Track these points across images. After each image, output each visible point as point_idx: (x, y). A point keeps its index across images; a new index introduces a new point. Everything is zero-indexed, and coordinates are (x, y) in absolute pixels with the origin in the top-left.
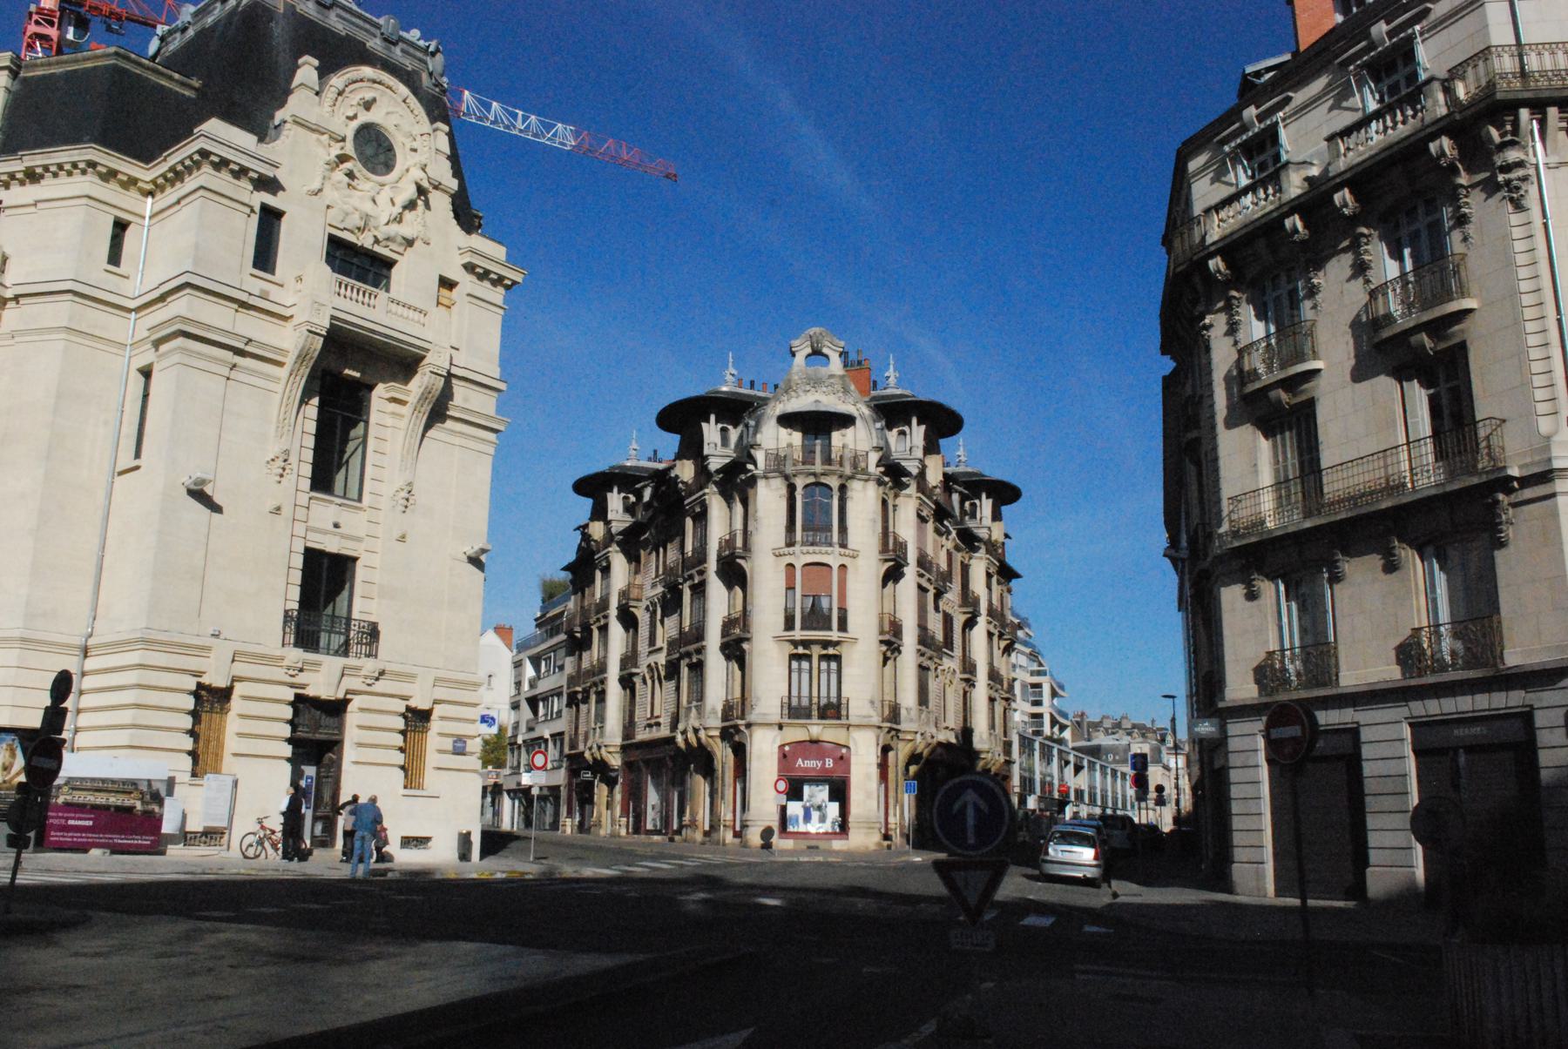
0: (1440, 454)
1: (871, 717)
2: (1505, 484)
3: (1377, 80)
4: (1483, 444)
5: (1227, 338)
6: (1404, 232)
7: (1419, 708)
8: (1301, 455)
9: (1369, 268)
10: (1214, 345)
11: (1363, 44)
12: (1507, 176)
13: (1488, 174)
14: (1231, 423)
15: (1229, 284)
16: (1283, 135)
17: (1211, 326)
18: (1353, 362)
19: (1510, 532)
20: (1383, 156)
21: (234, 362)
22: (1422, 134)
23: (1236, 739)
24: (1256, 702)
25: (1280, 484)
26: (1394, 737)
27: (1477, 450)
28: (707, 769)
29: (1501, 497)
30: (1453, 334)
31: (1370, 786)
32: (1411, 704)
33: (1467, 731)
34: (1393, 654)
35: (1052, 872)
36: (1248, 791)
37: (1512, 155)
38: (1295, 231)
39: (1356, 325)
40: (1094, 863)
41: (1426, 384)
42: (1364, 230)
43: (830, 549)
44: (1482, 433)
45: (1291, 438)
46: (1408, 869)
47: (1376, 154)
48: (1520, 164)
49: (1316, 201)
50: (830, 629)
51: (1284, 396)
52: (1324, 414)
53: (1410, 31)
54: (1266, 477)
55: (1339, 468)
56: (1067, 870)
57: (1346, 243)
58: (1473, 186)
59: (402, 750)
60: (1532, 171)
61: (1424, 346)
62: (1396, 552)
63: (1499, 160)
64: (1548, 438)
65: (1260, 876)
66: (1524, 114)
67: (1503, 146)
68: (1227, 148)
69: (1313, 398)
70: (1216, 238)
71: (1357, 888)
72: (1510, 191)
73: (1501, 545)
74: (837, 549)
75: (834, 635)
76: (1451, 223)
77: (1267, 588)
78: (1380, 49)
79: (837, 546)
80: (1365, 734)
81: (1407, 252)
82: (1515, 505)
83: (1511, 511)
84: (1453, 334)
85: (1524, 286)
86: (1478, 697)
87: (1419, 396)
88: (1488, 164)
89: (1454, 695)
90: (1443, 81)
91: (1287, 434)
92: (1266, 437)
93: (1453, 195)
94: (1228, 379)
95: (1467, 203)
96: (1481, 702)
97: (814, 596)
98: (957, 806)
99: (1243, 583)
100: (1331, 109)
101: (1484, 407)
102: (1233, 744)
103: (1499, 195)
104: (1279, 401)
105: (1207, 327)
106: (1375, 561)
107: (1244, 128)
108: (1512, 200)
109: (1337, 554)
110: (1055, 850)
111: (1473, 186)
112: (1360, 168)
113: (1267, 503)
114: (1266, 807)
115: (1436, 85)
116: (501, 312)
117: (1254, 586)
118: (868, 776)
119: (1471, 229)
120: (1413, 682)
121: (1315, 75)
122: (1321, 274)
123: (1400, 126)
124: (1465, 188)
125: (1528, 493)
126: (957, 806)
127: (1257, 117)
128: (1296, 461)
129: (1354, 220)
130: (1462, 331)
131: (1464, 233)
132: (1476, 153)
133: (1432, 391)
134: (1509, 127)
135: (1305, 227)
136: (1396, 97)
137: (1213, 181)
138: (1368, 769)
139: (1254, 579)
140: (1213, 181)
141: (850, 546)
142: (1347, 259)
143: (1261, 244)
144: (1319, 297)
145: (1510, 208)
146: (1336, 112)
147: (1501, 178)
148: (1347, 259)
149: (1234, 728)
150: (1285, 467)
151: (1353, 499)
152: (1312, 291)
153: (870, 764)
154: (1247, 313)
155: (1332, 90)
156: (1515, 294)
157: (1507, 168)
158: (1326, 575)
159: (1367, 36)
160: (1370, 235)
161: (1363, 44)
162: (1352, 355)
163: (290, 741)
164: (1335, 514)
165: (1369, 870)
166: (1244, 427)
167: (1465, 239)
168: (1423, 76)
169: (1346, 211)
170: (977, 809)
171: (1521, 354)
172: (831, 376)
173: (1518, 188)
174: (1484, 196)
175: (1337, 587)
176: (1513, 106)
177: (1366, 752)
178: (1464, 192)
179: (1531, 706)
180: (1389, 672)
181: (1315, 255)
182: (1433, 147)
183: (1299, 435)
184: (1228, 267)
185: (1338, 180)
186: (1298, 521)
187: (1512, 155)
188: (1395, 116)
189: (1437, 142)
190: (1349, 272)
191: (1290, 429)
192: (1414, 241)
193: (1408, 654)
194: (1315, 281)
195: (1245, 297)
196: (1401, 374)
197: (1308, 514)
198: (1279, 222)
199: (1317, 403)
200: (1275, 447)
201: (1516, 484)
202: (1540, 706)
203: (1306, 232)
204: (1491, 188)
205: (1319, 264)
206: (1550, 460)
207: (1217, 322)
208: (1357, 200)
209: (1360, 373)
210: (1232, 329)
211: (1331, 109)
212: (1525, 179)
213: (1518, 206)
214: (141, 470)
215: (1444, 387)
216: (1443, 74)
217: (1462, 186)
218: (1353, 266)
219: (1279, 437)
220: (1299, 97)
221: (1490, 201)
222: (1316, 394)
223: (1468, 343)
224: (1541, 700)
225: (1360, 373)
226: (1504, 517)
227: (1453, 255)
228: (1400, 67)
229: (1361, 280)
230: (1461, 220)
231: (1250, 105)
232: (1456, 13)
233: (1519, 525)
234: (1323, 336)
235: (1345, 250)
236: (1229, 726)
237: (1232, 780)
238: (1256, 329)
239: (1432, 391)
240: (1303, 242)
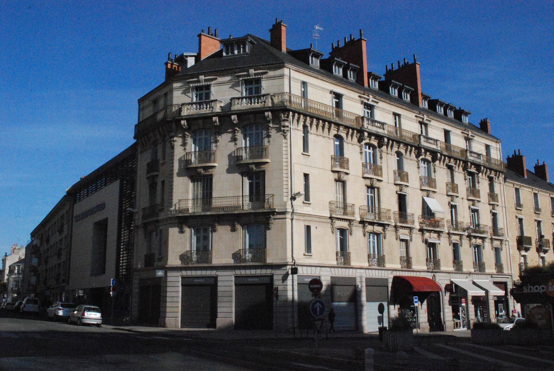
0: (251, 200)
2: (273, 213)
3: (246, 85)
4: (266, 201)
5: (181, 147)
6: (248, 132)
7: (238, 272)
8: (203, 190)
9: (237, 140)
10: (176, 147)
11: (245, 73)
12: (284, 129)
13: (278, 126)
14: (179, 175)
15: (185, 130)
16: (213, 89)
17: (176, 141)
18: (227, 167)
19: (272, 226)
20: (250, 110)
21: (163, 93)
22: (264, 109)
23: (170, 277)
24: (180, 266)
25: (195, 199)
26: (230, 280)
27: (264, 202)
28: (345, 264)
29: (272, 216)
30: (261, 168)
31: (219, 294)
32: (182, 271)
33: (198, 280)
34: (231, 256)
35: (86, 322)
36: (174, 294)
37: (287, 124)
38: (216, 122)
39: (230, 156)
40: (101, 318)
41: (249, 179)
42: (237, 129)
44: (266, 198)
45: (201, 184)
46: (231, 319)
47: (248, 109)
48: (288, 127)
49: (225, 115)
51: (202, 172)
52: (215, 181)
53: (262, 76)
54: (190, 196)
55: (225, 198)
56: (91, 321)
57: (230, 130)
58: (274, 128)
60: (289, 129)
61: (253, 169)
62: (236, 226)
63: (283, 124)
64: (286, 203)
65: (176, 321)
66: (291, 113)
67: (284, 120)
68: (191, 85)
69: (212, 174)
70: (185, 114)
71: (213, 324)
72: (284, 133)
73: (269, 229)
76: (265, 136)
77: (187, 230)
78: (251, 77)
80: (219, 279)
81: (248, 139)
82: (274, 219)
83: (273, 220)
84: (261, 168)
85: (284, 160)
86: (268, 270)
87: (247, 182)
88: (279, 123)
89: (196, 270)
90: (272, 96)
91: (199, 183)
92: (192, 183)
93: (268, 128)
94: (180, 160)
95: (271, 132)
96: (258, 272)
99: (178, 227)
100: (230, 88)
101: (268, 191)
102: (169, 279)
103: (281, 133)
104: (201, 173)
105: (174, 141)
106: (228, 228)
107: (199, 81)
108: (284, 135)
109: (216, 224)
110: (87, 314)
111: (274, 128)
112: (242, 111)
113: (190, 204)
114: (180, 300)
115: (269, 96)
117: (183, 229)
119: (271, 139)
120: (238, 265)
122: (220, 137)
123: (256, 103)
124: (271, 128)
125: (278, 216)
126: (315, 306)
127: (204, 80)
128: (201, 192)
130: (265, 167)
131: (269, 140)
132: (277, 119)
133: (250, 181)
134: (286, 115)
135: (219, 122)
136: (257, 95)
137: (182, 93)
138: (219, 289)
139: (183, 227)
140: (182, 93)
142: (229, 136)
143: (200, 122)
144: (218, 144)
145: (283, 138)
146: (231, 89)
147: (282, 129)
148: (229, 136)
149: (169, 274)
150: (197, 193)
151: (223, 208)
152: (216, 141)
154: (190, 141)
155: (231, 82)
156: (281, 162)
157: (284, 127)
158: (210, 230)
159: (248, 71)
160: (239, 131)
161: (245, 73)
162: (228, 164)
164: (219, 212)
165: (218, 319)
166: (186, 177)
167: (269, 142)
168: (263, 92)
169: (235, 122)
171: (281, 179)
173: (286, 133)
174: (276, 132)
175: (214, 234)
176: (289, 110)
177: (219, 284)
178: (271, 128)
179: (273, 274)
180: (230, 261)
181: (219, 131)
182: (266, 114)
183: (204, 183)
184: (187, 125)
185: (234, 112)
186: (199, 211)
187: (287, 124)
188: (255, 100)
189: (268, 113)
190: (230, 140)
191: (201, 181)
192: (251, 136)
193: (236, 256)
194: (218, 138)
195: (190, 135)
196: (243, 174)
197: (203, 210)
198: (211, 117)
199: (213, 176)
200: (194, 186)
201: (276, 213)
202: (276, 274)
203: (219, 123)
204: (279, 130)
205: (220, 134)
206: (286, 209)
207: (178, 141)
208: (238, 120)
209: (229, 171)
210: (184, 144)
211: (230, 88)
212: (288, 131)
213: (285, 137)
215: (254, 181)
216: (272, 94)
217: (270, 127)
218: (231, 138)
219: (196, 183)
220: (220, 79)
221: (277, 134)
222: (214, 173)
223: (266, 171)
224: (276, 272)
225: (229, 171)
226: (271, 222)
227: (264, 146)
228: (254, 84)
229: (233, 143)
230: (269, 136)
231: (203, 75)
232: (275, 77)
233: (275, 224)
234: (218, 155)
235: (229, 132)
236: (168, 273)
237: (167, 291)
238: (191, 147)
239: (250, 181)
240: (217, 126)
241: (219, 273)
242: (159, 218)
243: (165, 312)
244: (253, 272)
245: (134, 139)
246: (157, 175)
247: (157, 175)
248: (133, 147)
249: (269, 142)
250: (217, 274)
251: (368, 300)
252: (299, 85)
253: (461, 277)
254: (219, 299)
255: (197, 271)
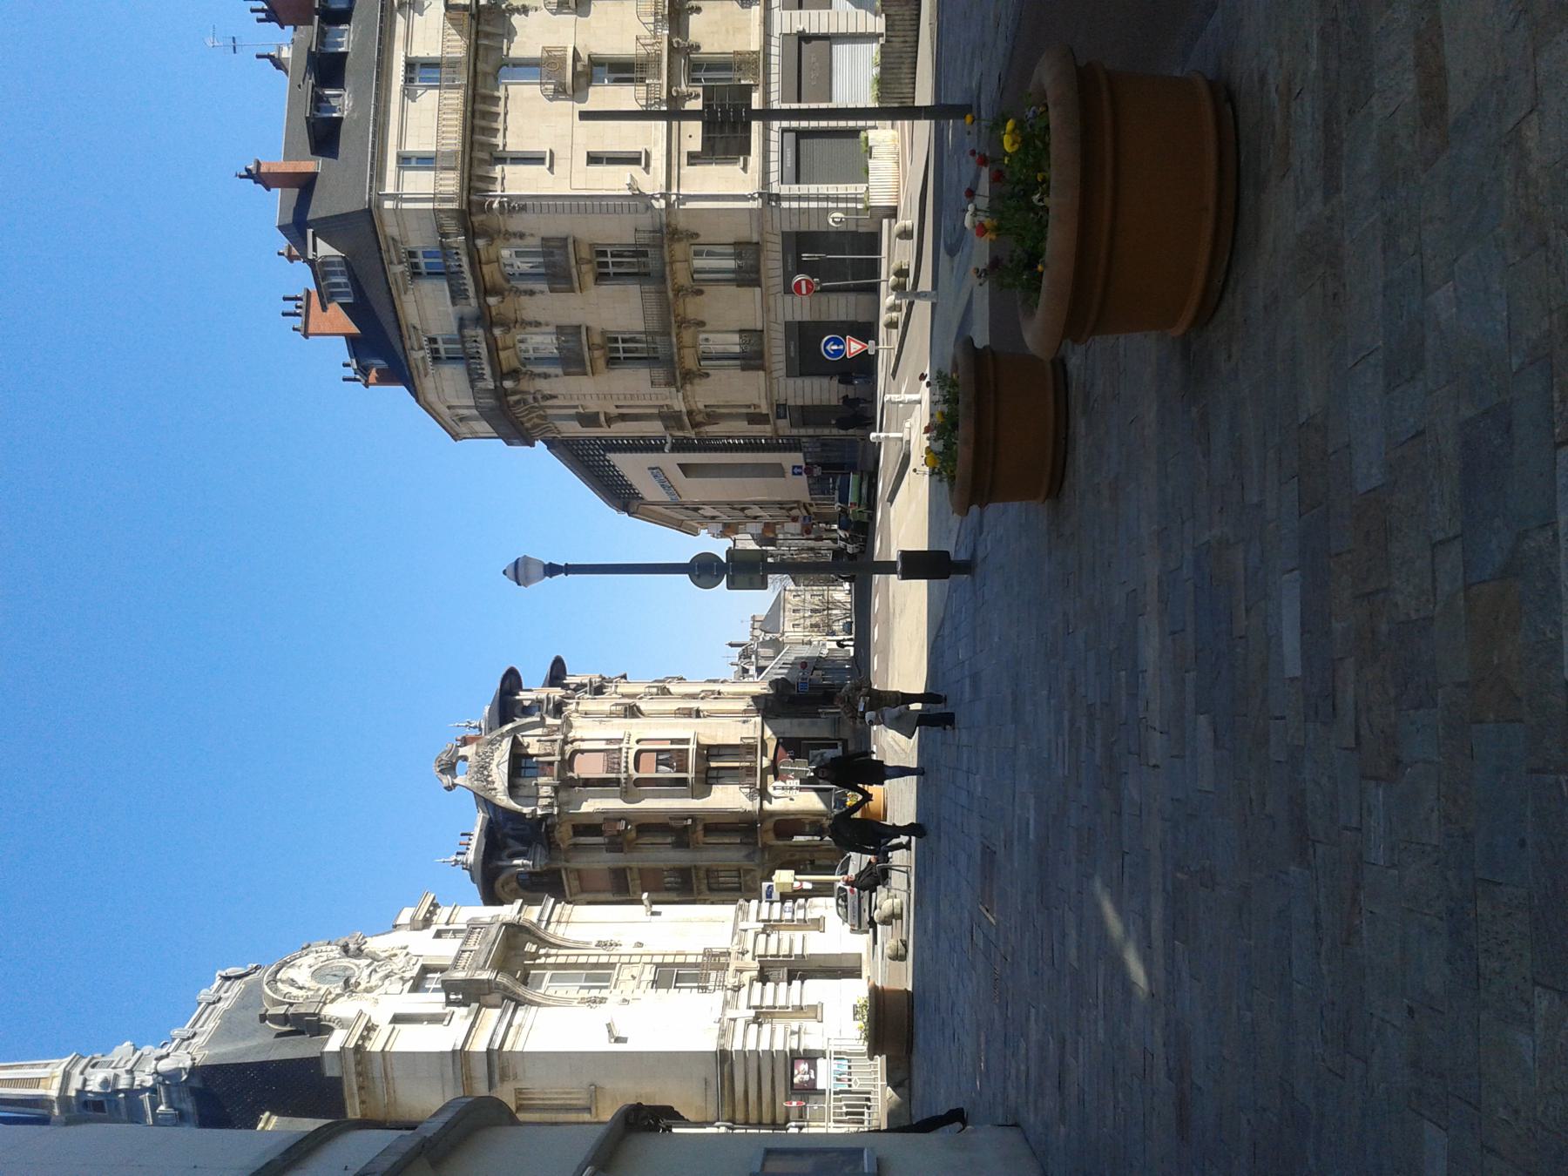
1: (755, 723)
32: (773, 6)
43: (624, 750)
50: (687, 750)
59: (777, 984)
74: (624, 745)
75: (692, 747)
79: (621, 745)
80: (789, 318)
97: (657, 764)
98: (832, 352)
116: (458, 908)
118: (800, 725)
121: (393, 22)
126: (832, 352)
129: (368, 1034)
141: (622, 737)
153: (791, 723)
163: (790, 983)
167: (532, 235)
170: (834, 344)
172: (477, 753)
177: (798, 318)
214: (553, 149)
241: (776, 31)
242: (684, 410)
243: (858, 43)
244: (774, 156)
245: (534, 446)
246: (605, 413)
247: (605, 413)
248: (551, 444)
249: (532, 235)
250: (778, 36)
251: (830, 100)
252: (409, 175)
253: (795, 219)
254: (824, 318)
255: (772, 81)
